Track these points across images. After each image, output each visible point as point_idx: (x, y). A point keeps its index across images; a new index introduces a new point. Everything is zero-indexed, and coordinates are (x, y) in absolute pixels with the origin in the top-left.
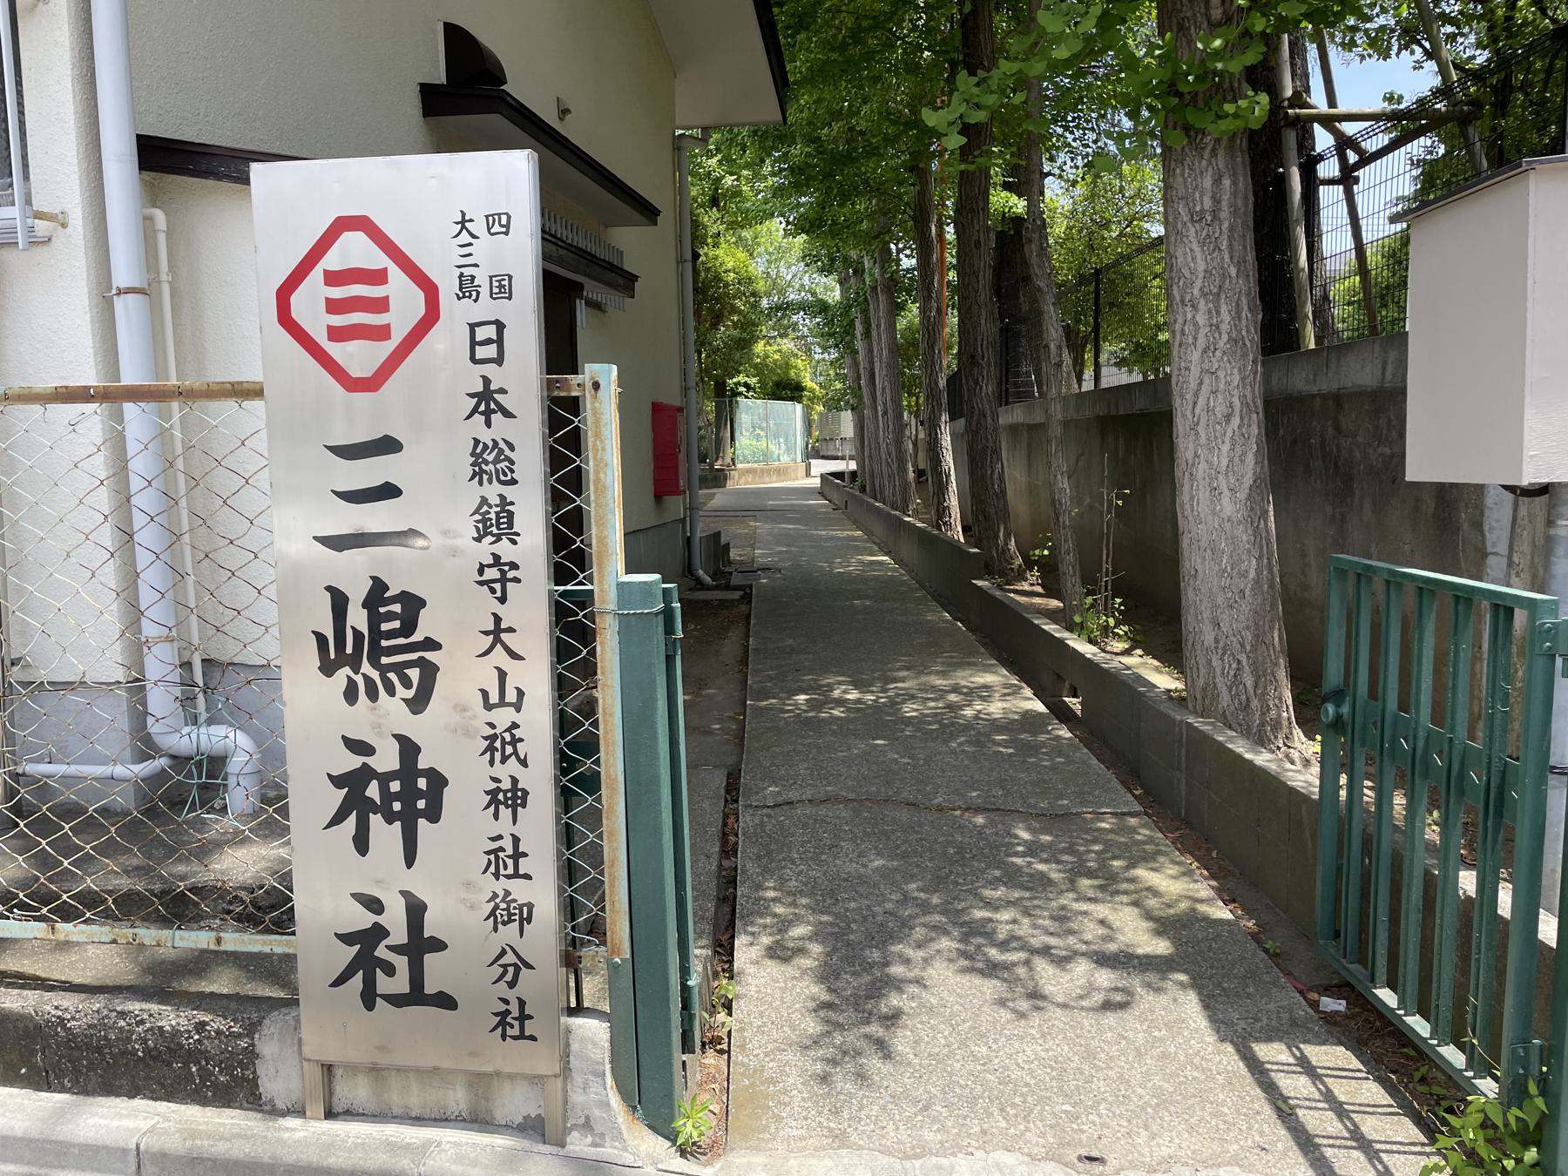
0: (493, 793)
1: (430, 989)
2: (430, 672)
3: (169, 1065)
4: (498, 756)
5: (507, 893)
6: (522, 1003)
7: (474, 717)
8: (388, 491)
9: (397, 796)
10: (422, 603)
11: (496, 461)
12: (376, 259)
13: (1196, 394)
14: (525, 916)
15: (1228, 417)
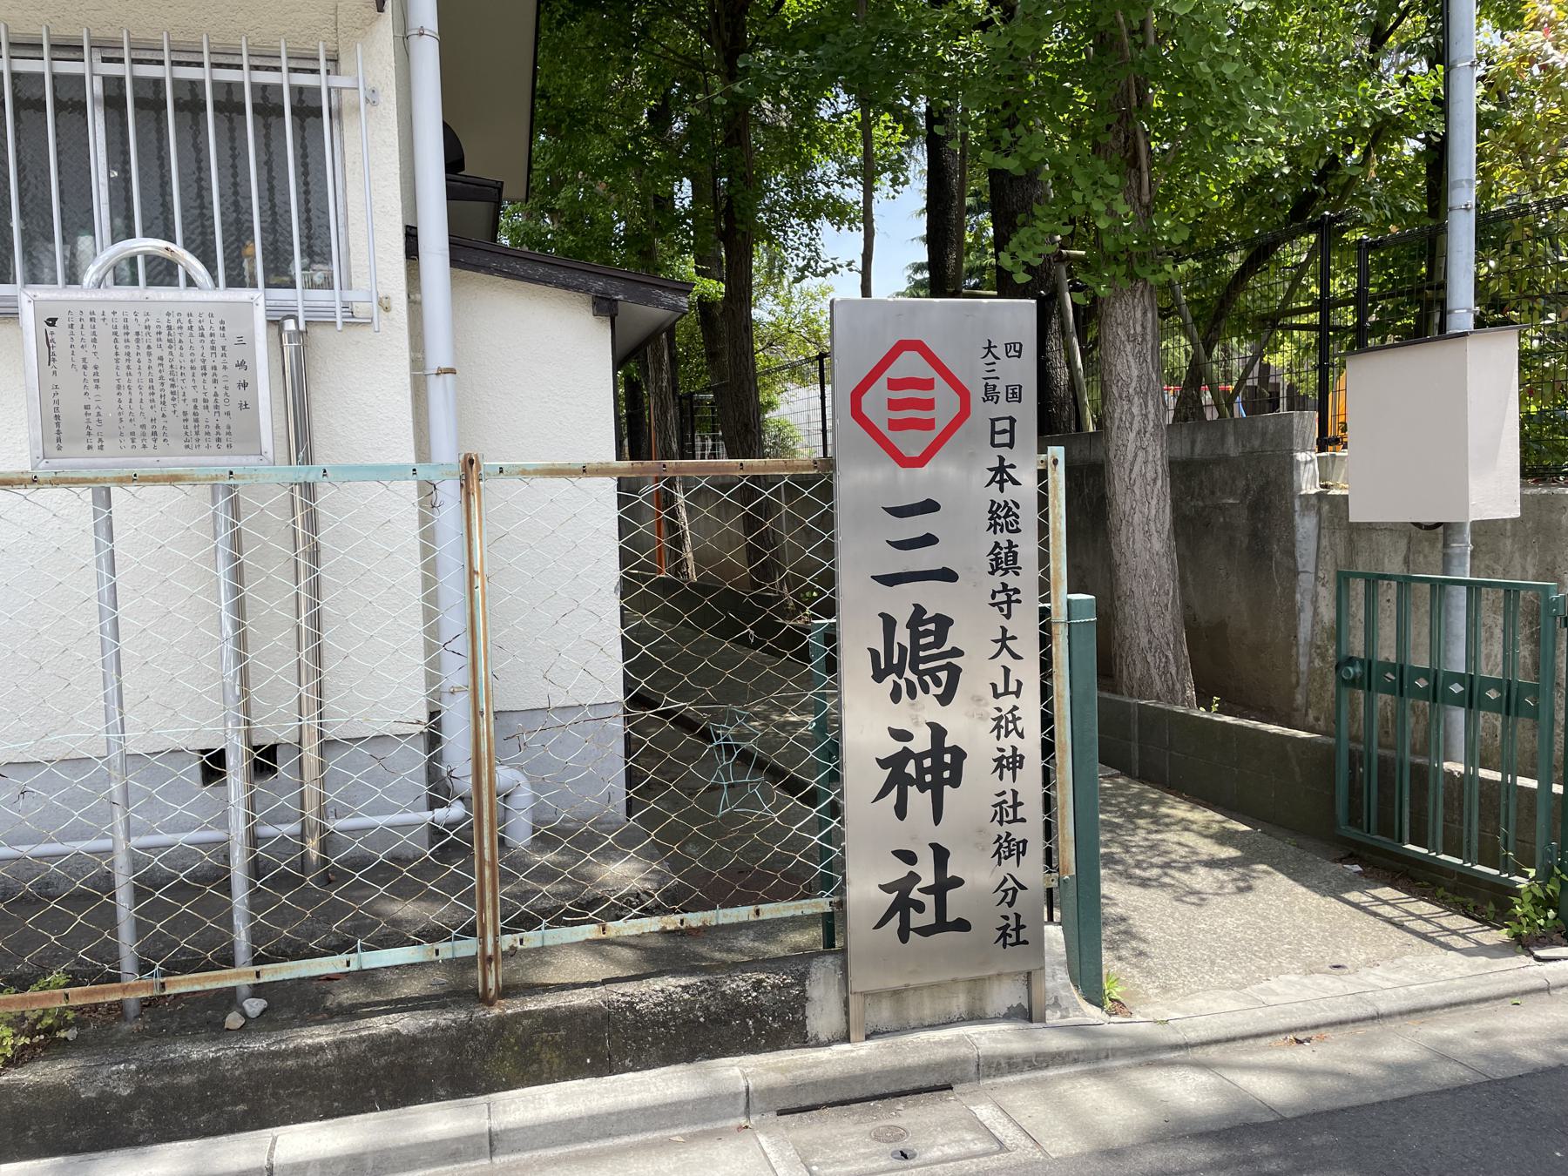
0: (999, 760)
1: (950, 918)
2: (954, 672)
3: (727, 1023)
4: (1003, 732)
5: (1009, 834)
6: (1018, 916)
7: (987, 704)
8: (929, 540)
9: (928, 771)
10: (951, 622)
11: (1006, 516)
12: (925, 371)
13: (1133, 464)
14: (1021, 848)
15: (1155, 481)
